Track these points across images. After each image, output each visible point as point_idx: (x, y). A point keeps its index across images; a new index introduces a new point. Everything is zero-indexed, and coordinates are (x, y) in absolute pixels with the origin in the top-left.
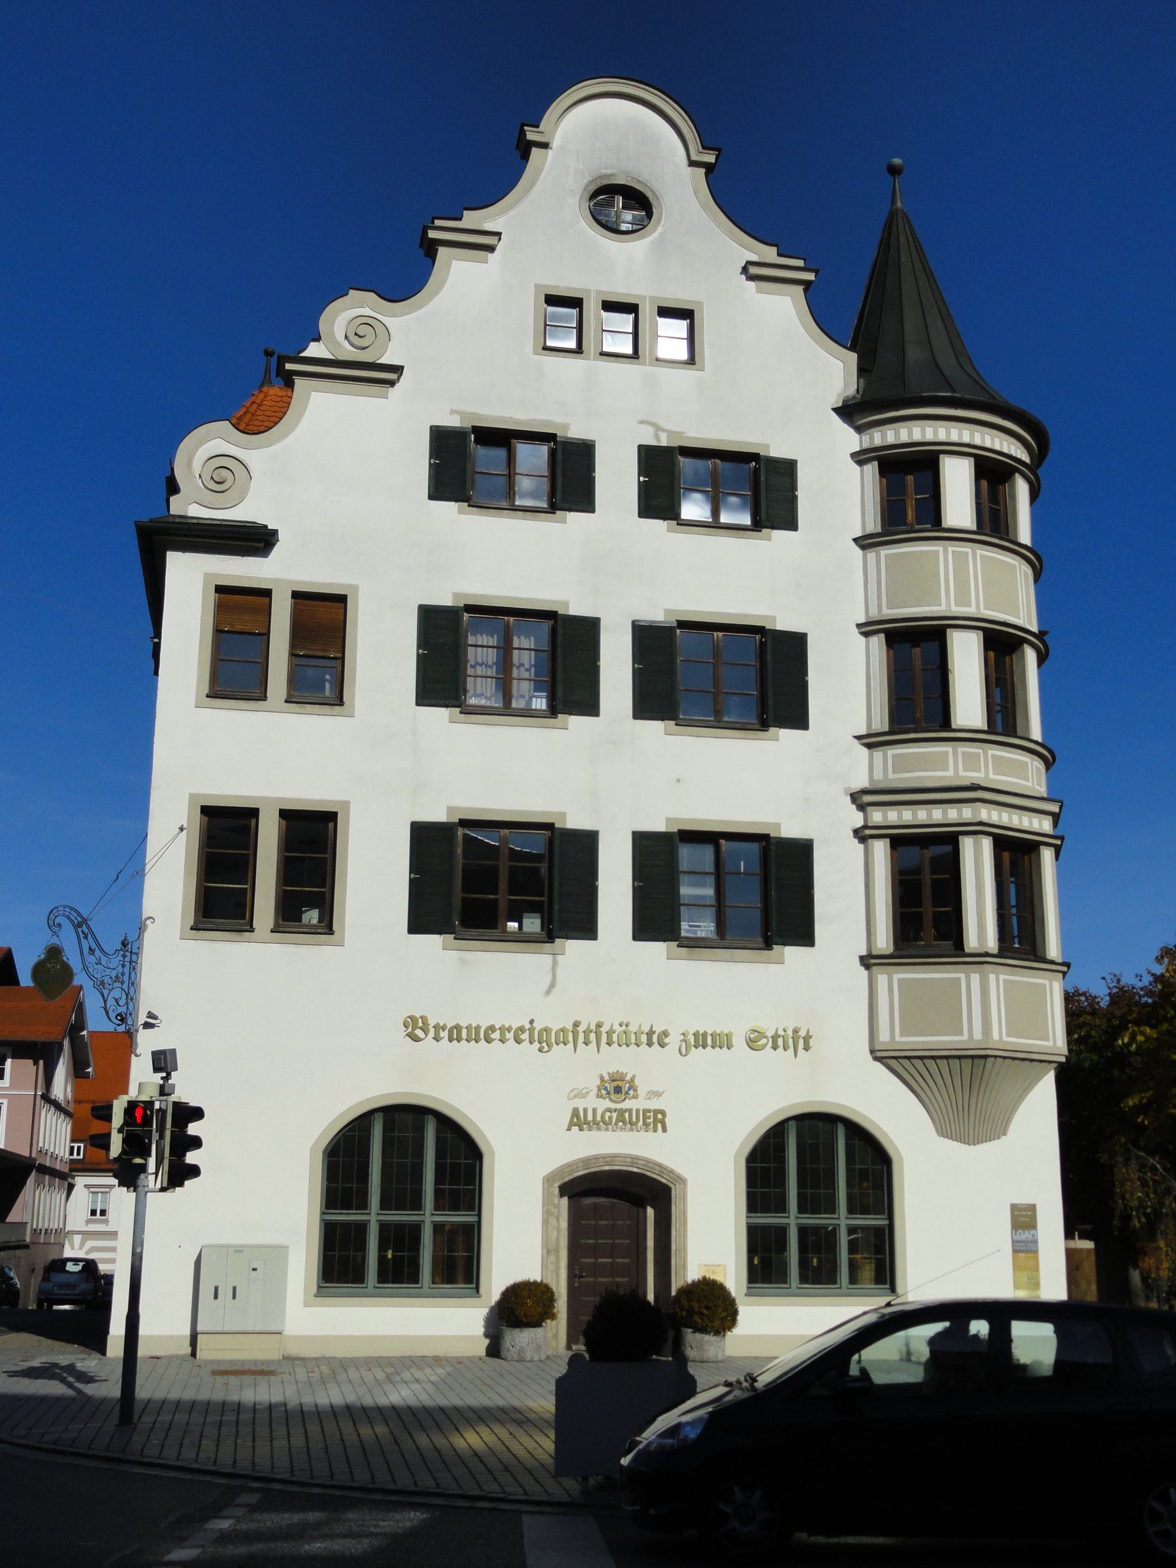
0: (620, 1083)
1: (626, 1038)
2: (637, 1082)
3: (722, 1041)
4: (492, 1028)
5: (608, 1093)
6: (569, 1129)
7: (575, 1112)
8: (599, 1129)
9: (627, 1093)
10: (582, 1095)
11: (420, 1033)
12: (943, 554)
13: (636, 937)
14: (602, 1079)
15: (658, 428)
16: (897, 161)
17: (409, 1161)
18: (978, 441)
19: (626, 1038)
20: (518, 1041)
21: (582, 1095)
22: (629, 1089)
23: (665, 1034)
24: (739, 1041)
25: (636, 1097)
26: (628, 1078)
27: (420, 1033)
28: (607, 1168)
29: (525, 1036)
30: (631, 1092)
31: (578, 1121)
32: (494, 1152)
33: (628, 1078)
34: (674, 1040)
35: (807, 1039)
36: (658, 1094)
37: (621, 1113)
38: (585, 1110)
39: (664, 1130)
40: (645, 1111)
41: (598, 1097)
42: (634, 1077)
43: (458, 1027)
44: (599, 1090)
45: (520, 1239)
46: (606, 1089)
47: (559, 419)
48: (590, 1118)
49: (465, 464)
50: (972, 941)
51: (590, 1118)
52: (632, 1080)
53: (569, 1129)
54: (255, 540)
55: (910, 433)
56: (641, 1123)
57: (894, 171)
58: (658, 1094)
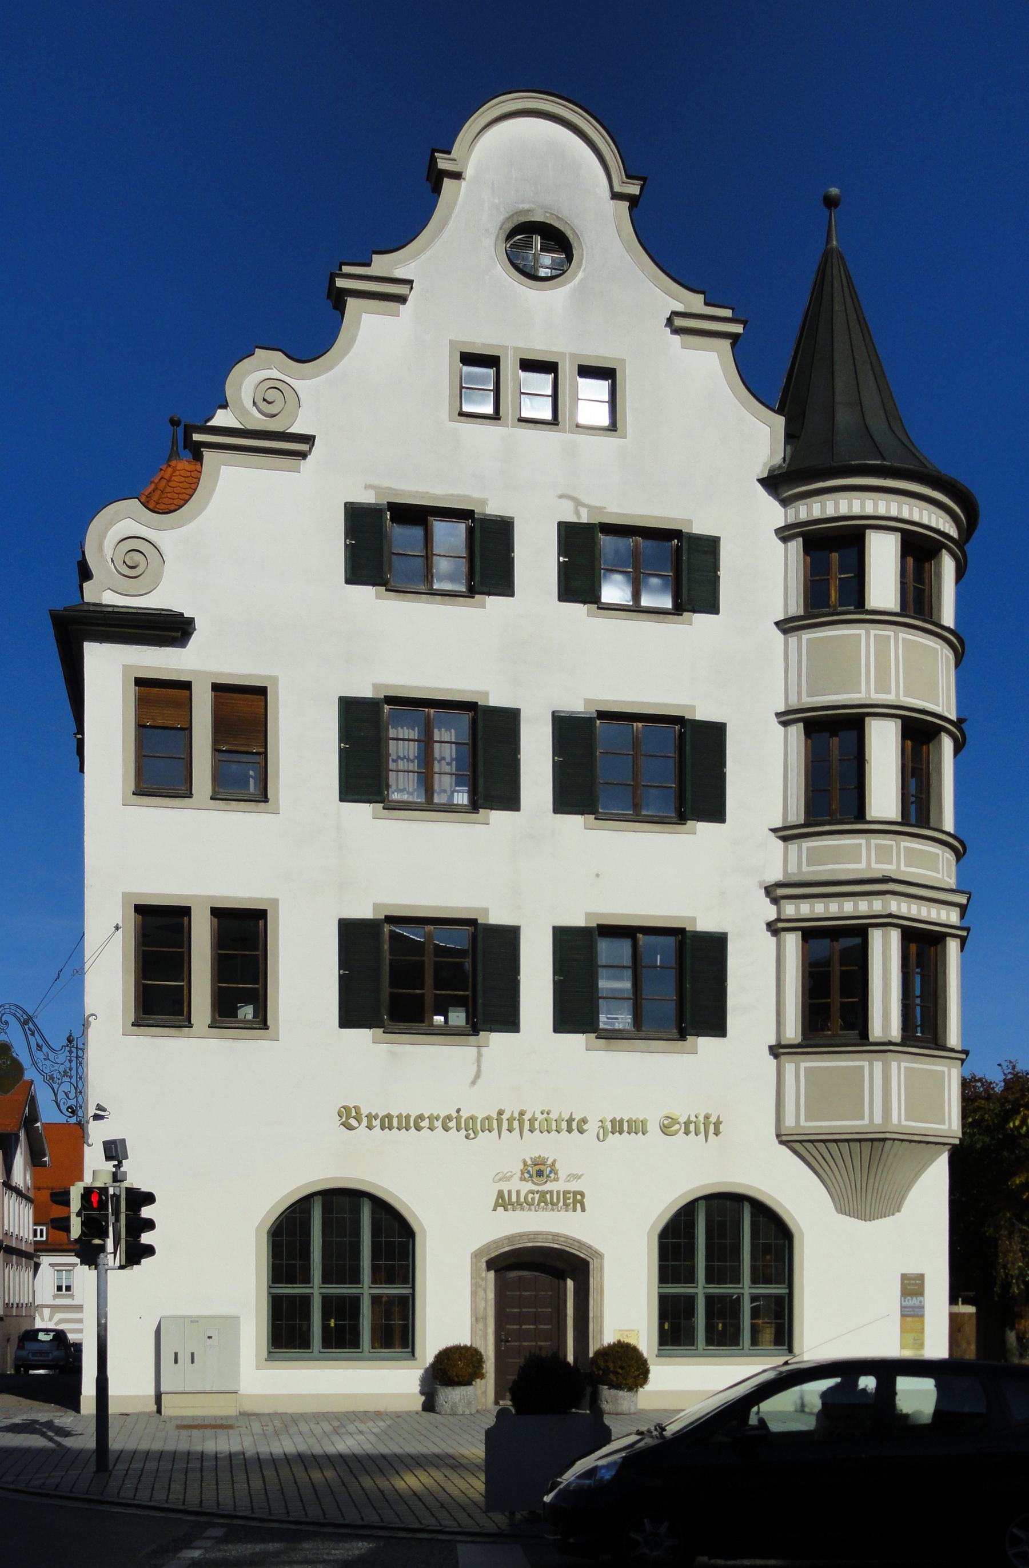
0: (542, 1167)
1: (547, 1125)
2: (557, 1166)
3: (637, 1127)
4: (421, 1117)
5: (531, 1176)
6: (495, 1210)
7: (500, 1194)
8: (522, 1209)
9: (548, 1176)
10: (506, 1178)
11: (353, 1122)
12: (864, 638)
13: (556, 1030)
15: (578, 503)
16: (834, 191)
17: (347, 1239)
18: (905, 515)
19: (547, 1125)
21: (506, 1178)
22: (551, 1172)
23: (584, 1121)
24: (653, 1127)
25: (556, 1180)
26: (549, 1162)
28: (530, 1244)
29: (452, 1124)
30: (552, 1175)
31: (503, 1202)
32: (425, 1232)
33: (549, 1162)
35: (717, 1124)
36: (577, 1177)
37: (542, 1194)
38: (510, 1192)
40: (565, 1193)
42: (555, 1161)
43: (389, 1117)
44: (522, 1173)
45: (451, 1307)
46: (528, 1172)
47: (476, 494)
48: (514, 1199)
49: (383, 544)
50: (876, 1031)
51: (514, 1199)
53: (495, 1210)
54: (171, 629)
55: (837, 507)
57: (831, 202)
58: (577, 1177)
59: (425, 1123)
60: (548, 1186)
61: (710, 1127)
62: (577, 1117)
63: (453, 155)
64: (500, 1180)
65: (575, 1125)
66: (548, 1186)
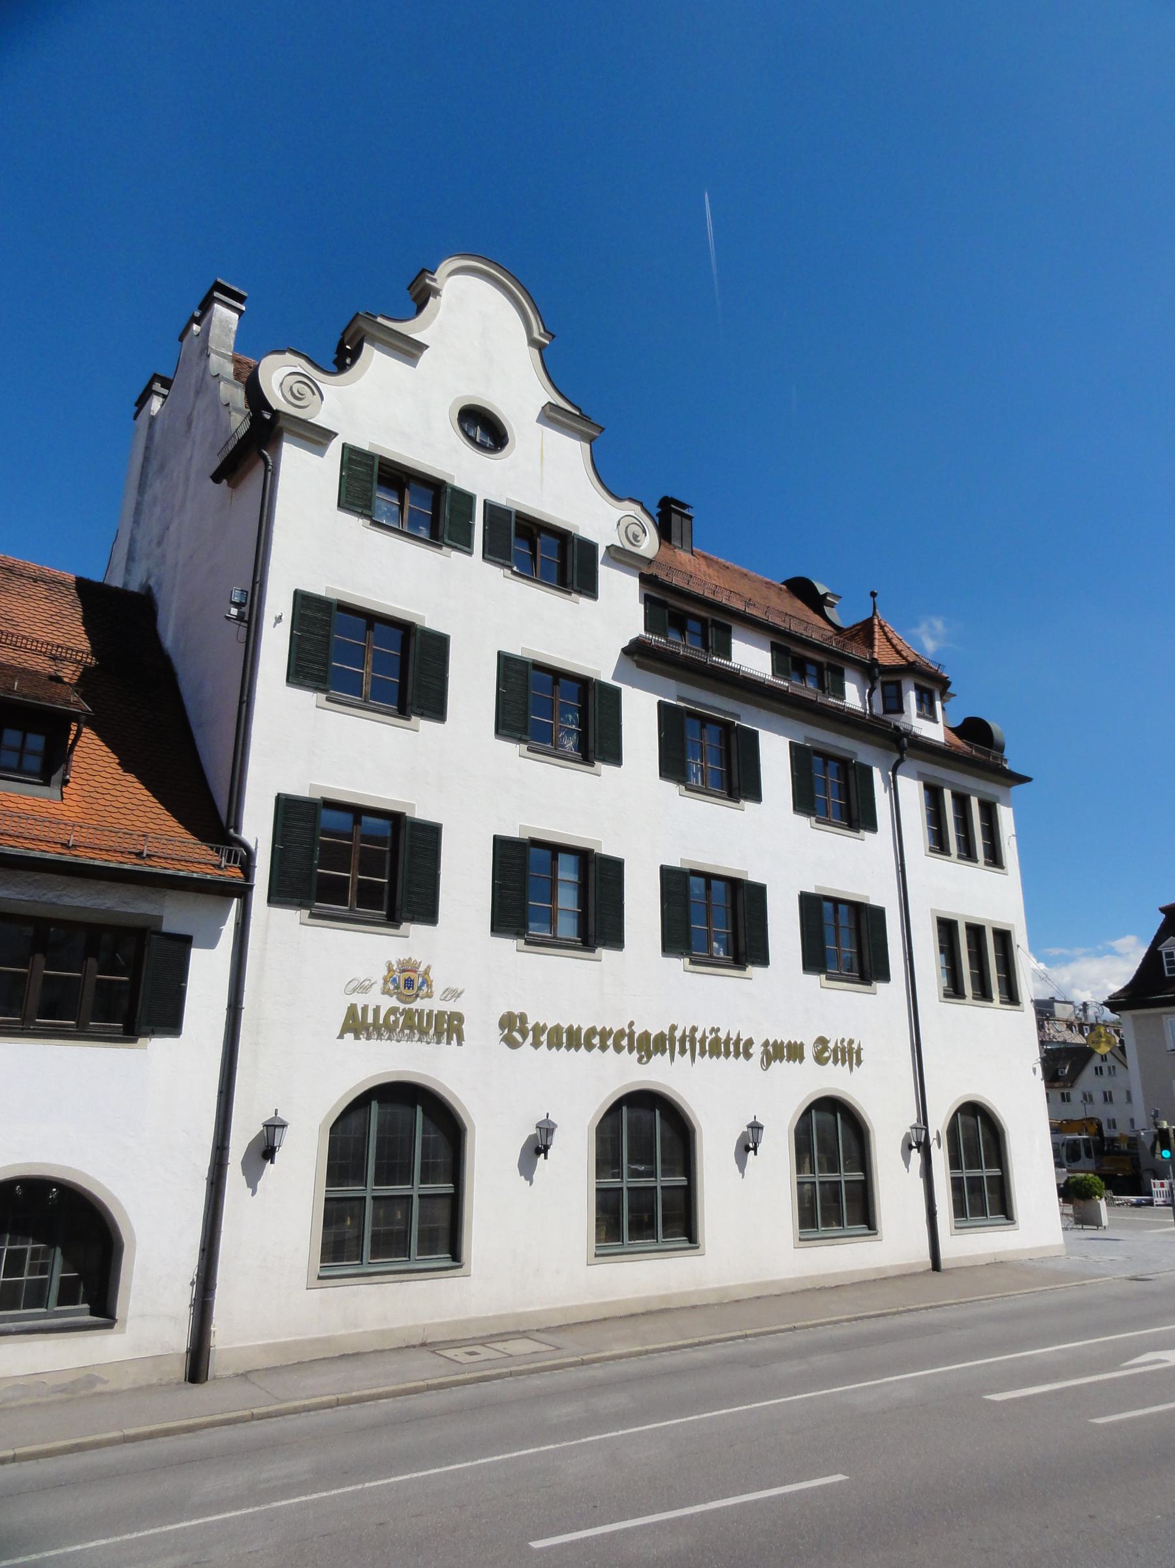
2: (432, 975)
4: (592, 1032)
5: (397, 988)
6: (341, 1037)
7: (352, 1009)
8: (380, 1036)
10: (363, 988)
11: (516, 1035)
14: (390, 969)
17: (417, 1189)
20: (618, 1048)
21: (363, 988)
23: (750, 1042)
24: (809, 1052)
25: (429, 996)
26: (422, 969)
27: (516, 1035)
29: (625, 1042)
31: (356, 1024)
33: (422, 969)
34: (757, 1050)
36: (456, 994)
37: (409, 1014)
38: (365, 1009)
39: (459, 1043)
40: (441, 1014)
41: (383, 993)
42: (429, 967)
43: (557, 1029)
44: (386, 982)
48: (370, 1020)
51: (370, 1020)
52: (427, 972)
53: (341, 1037)
56: (432, 1031)
58: (456, 994)
59: (596, 1041)
60: (418, 1005)
61: (849, 1055)
62: (744, 1037)
63: (435, 276)
64: (354, 990)
65: (743, 1049)
66: (418, 1005)
